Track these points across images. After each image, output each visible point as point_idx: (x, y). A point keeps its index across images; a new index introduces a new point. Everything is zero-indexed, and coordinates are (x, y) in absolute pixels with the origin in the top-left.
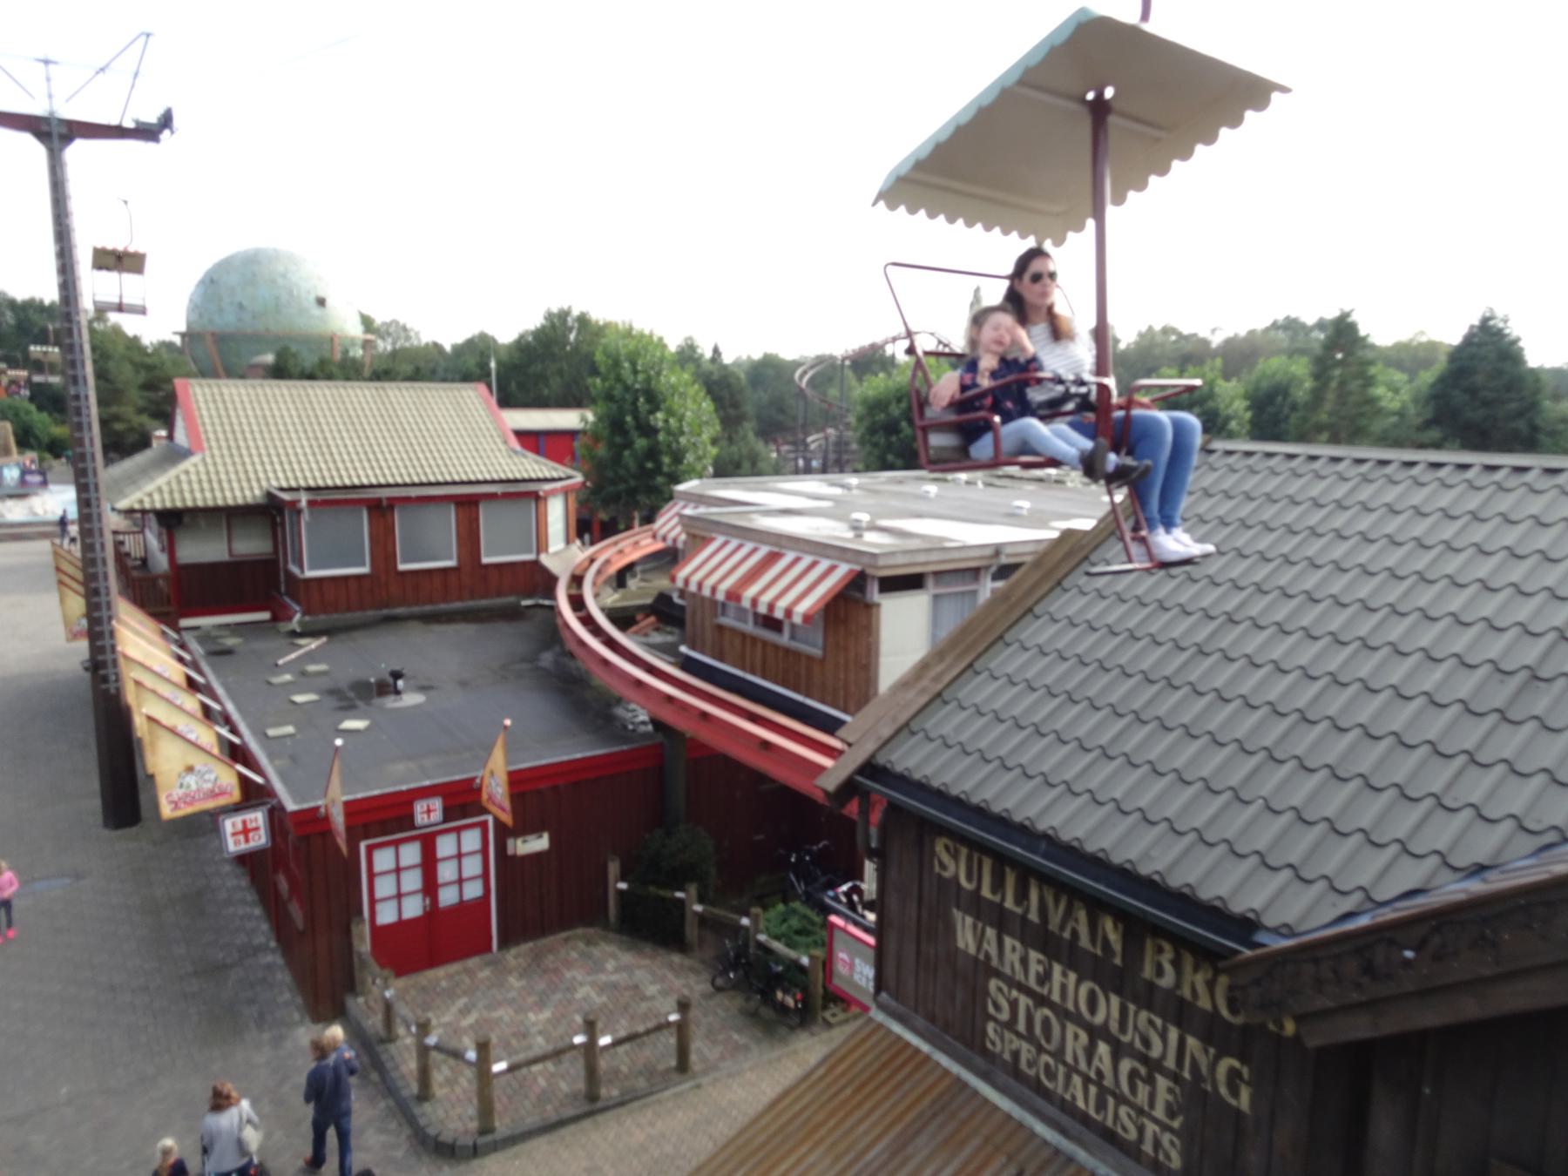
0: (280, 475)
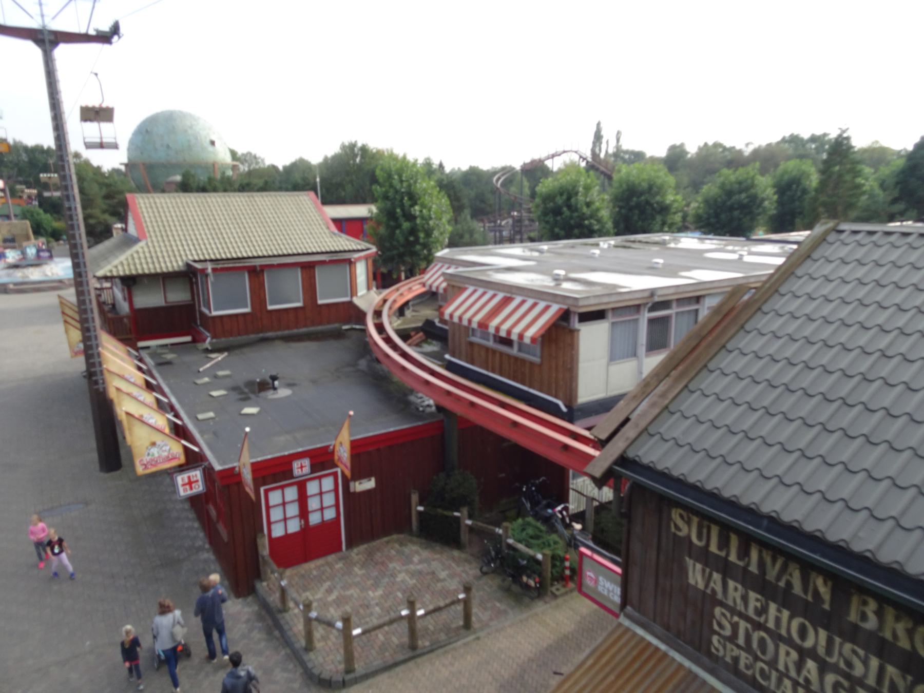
0: (194, 252)
